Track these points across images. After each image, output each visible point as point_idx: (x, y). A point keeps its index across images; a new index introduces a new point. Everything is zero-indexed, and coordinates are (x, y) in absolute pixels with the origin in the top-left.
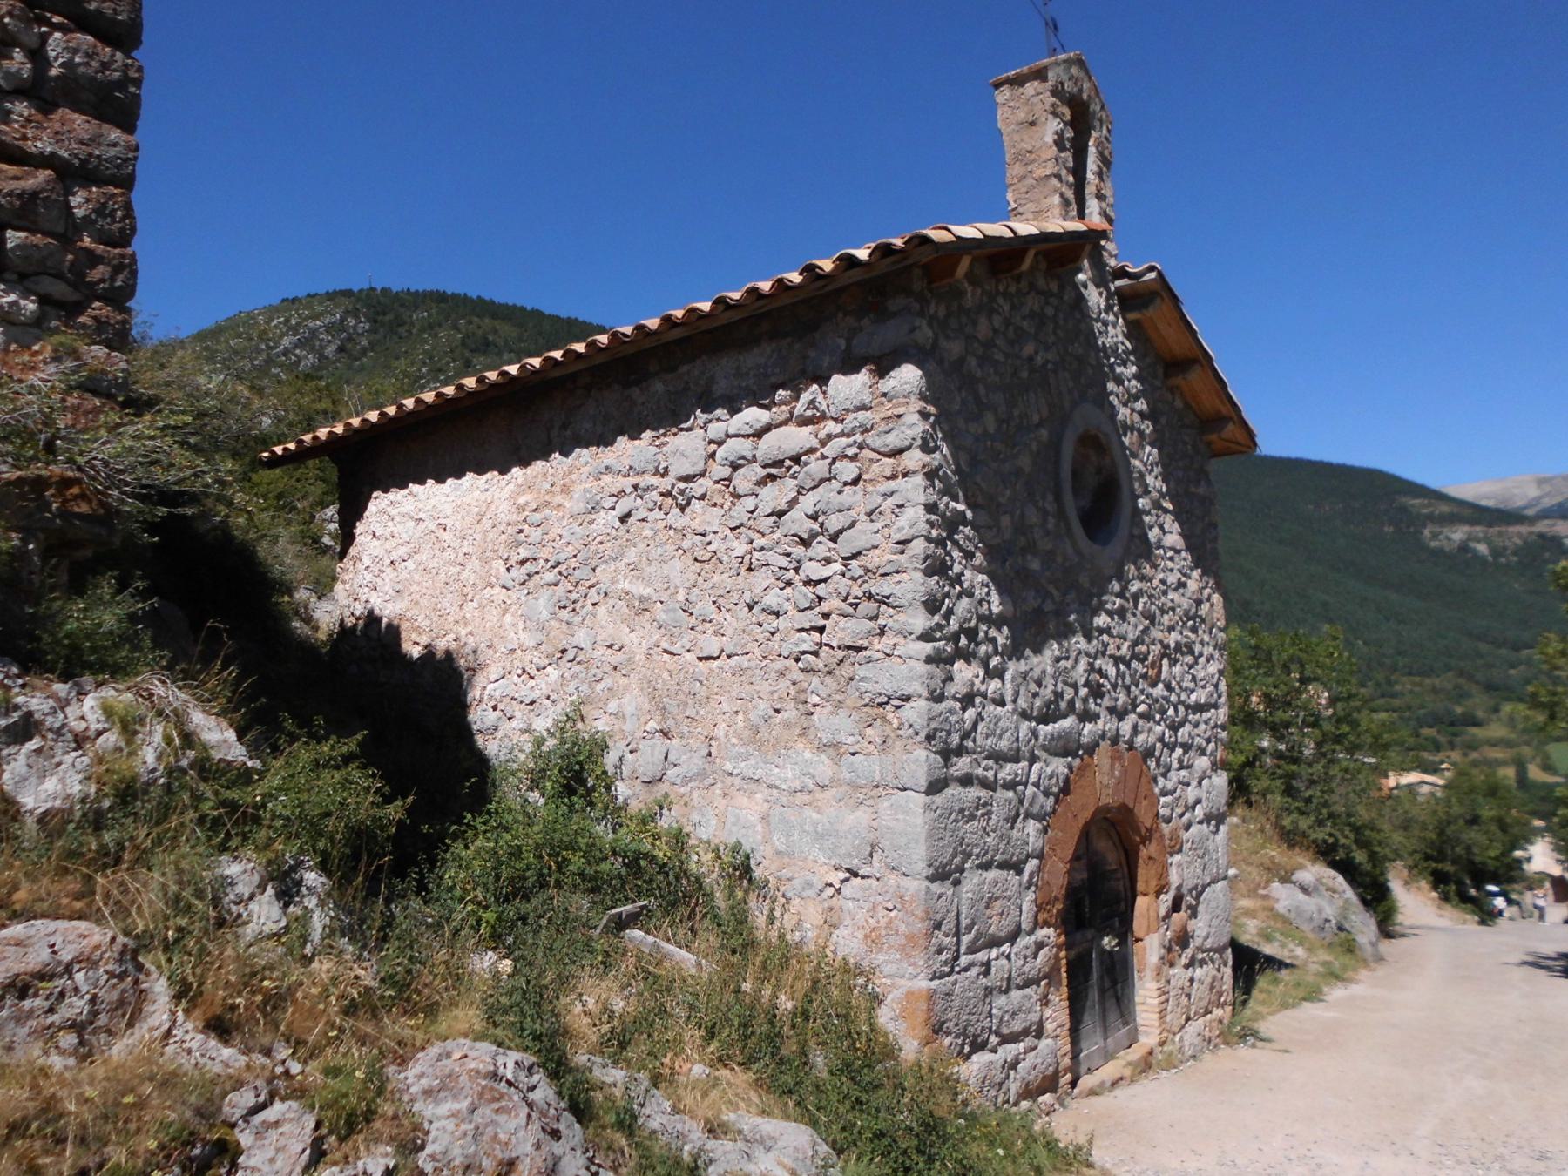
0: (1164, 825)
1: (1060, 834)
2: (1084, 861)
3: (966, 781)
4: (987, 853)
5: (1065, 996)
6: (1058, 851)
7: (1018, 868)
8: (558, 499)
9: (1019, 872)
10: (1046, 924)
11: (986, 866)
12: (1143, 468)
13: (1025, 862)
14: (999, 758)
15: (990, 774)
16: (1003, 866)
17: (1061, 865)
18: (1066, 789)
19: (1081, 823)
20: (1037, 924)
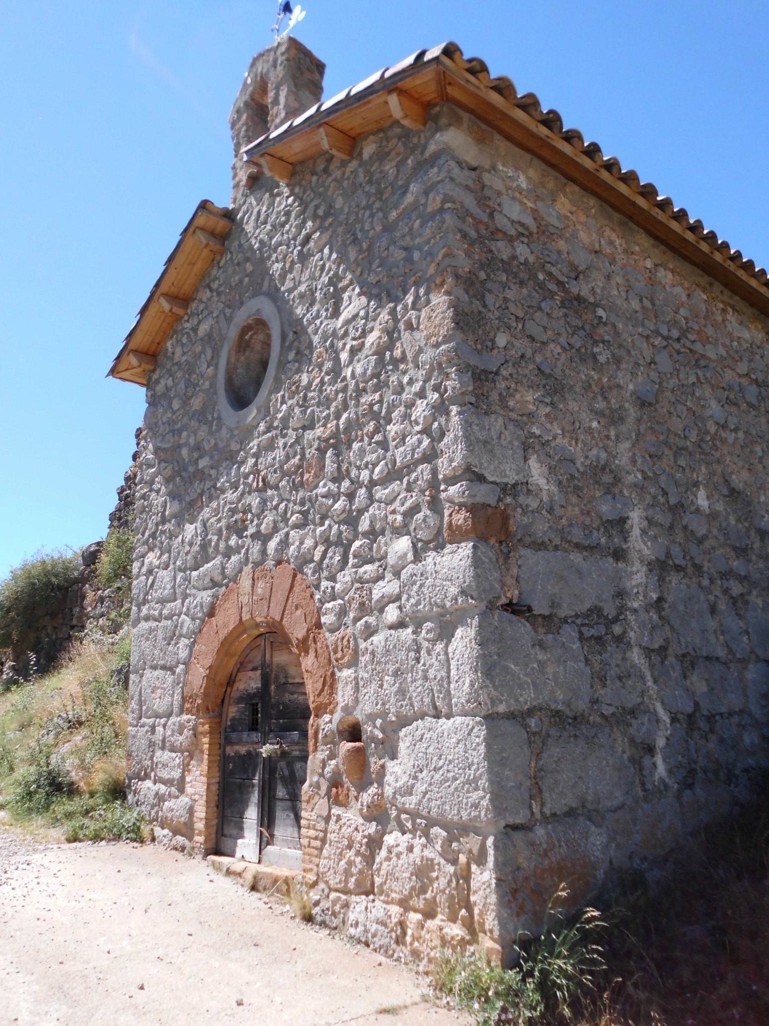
0: (327, 635)
1: (203, 647)
2: (259, 672)
3: (147, 618)
4: (154, 659)
5: (205, 773)
6: (201, 660)
7: (171, 669)
8: (713, 452)
9: (174, 673)
10: (189, 712)
11: (154, 668)
12: (433, 265)
13: (177, 667)
14: (162, 601)
15: (156, 613)
16: (164, 668)
17: (202, 670)
18: (211, 614)
19: (222, 636)
20: (181, 711)
